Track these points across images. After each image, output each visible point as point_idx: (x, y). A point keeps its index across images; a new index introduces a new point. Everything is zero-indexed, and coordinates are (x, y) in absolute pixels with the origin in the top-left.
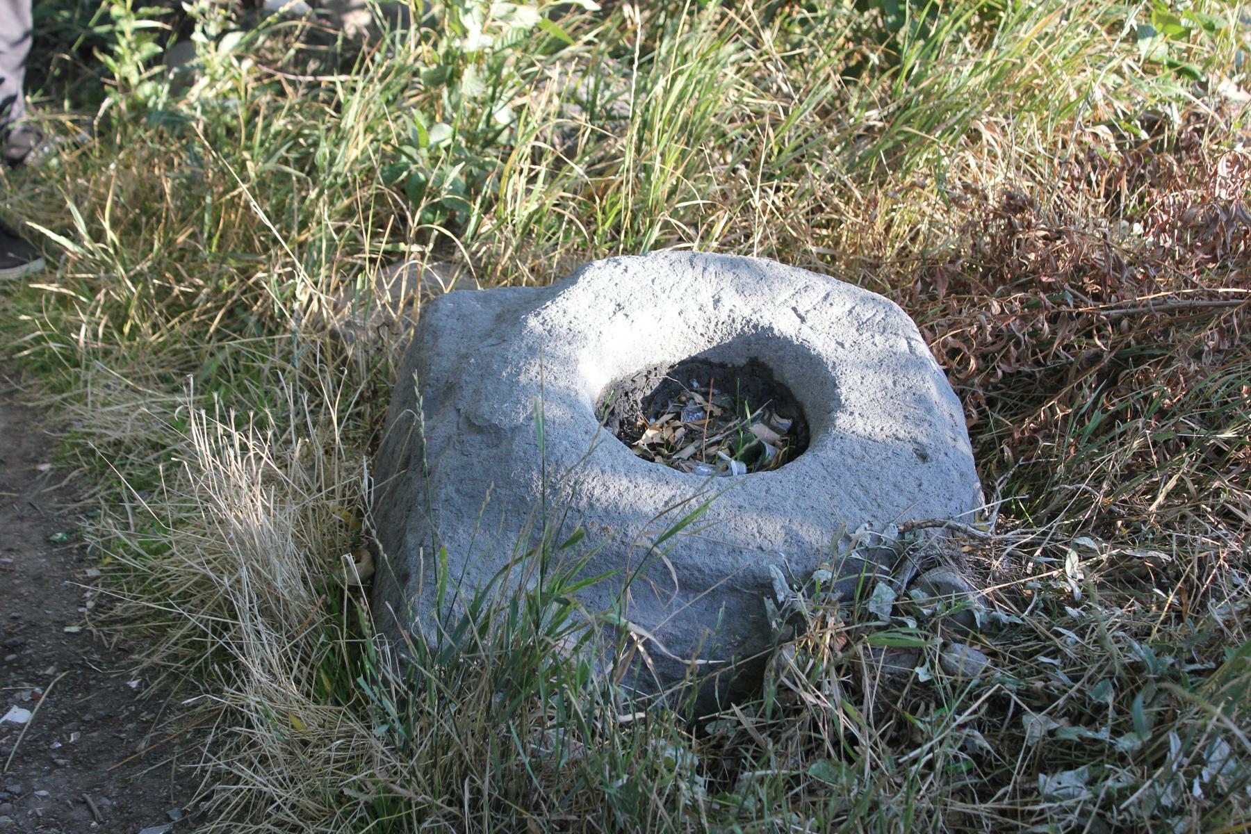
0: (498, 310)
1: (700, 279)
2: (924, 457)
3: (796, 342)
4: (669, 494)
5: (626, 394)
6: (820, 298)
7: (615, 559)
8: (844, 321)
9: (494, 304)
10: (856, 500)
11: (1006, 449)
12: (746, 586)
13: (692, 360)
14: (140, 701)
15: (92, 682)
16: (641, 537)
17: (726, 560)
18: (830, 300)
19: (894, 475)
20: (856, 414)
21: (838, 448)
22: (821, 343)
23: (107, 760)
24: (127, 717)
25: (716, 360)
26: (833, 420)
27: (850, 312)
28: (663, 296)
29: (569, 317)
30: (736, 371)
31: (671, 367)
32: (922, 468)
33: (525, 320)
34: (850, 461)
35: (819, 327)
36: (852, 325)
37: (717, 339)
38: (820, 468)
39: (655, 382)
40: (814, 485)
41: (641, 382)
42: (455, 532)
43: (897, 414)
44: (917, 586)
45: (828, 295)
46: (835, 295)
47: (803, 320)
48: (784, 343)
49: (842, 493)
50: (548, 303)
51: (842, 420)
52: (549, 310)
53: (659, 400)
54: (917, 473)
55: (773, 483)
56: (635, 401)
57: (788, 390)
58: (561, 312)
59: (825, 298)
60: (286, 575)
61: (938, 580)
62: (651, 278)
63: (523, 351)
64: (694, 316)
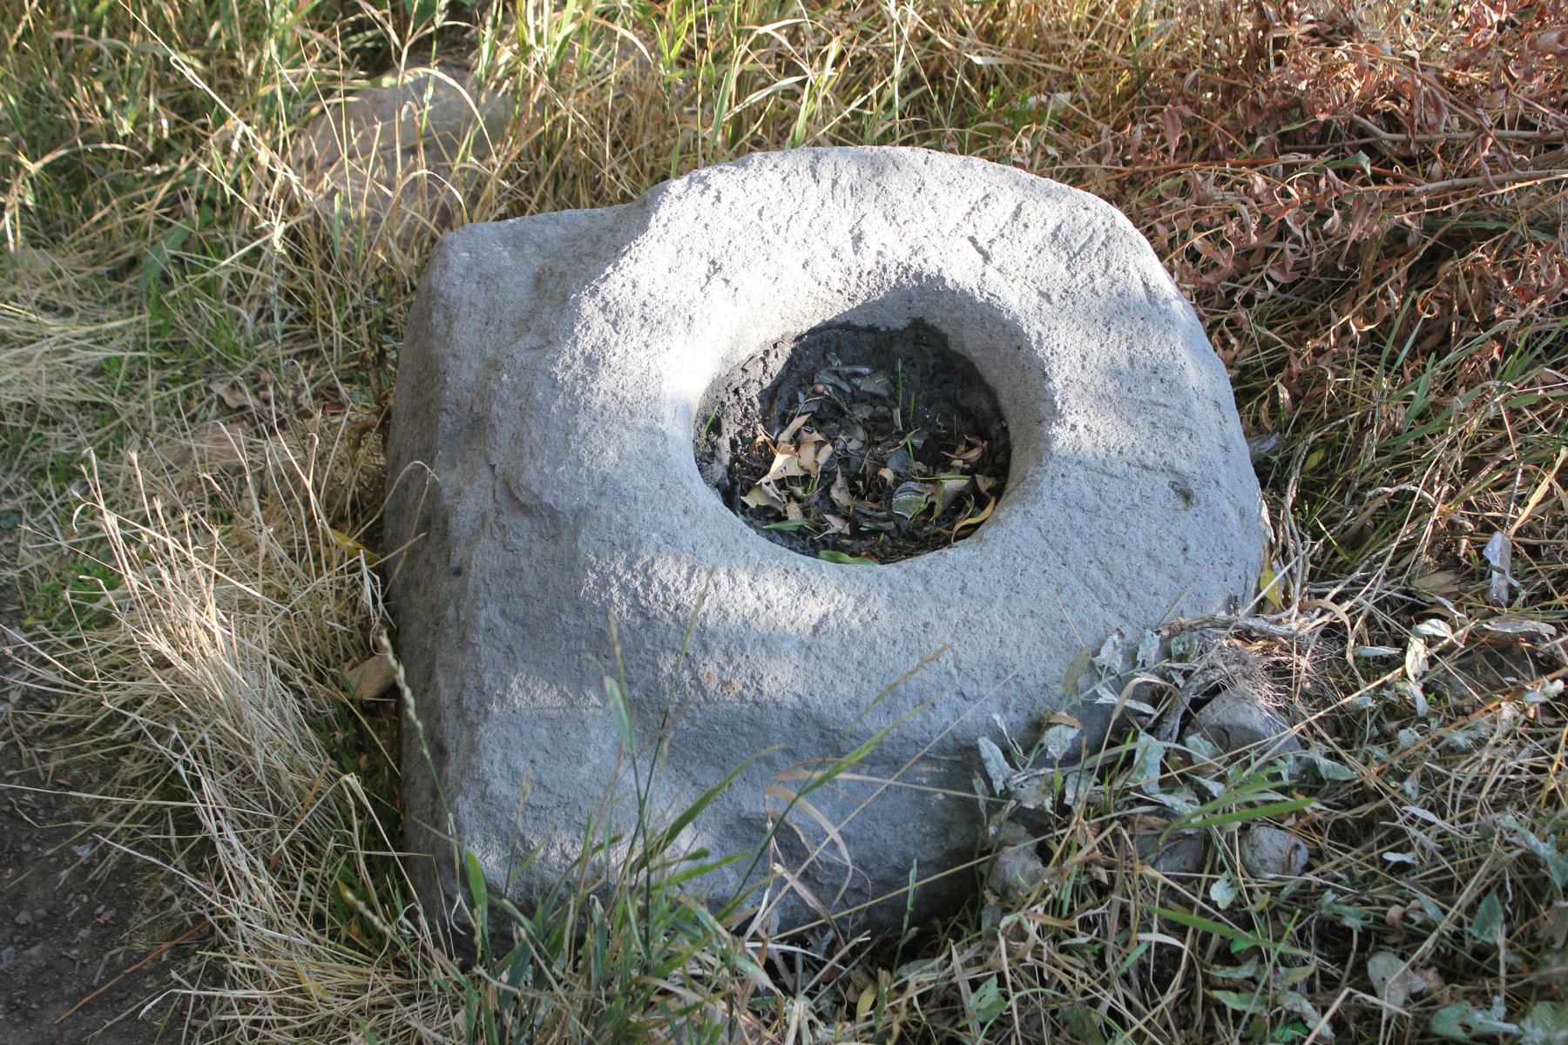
0: (537, 262)
1: (829, 202)
2: (1187, 496)
3: (980, 300)
4: (818, 612)
5: (736, 392)
6: (1007, 217)
7: (746, 729)
8: (1047, 254)
9: (529, 250)
10: (1095, 589)
11: (1281, 388)
12: (944, 751)
13: (828, 326)
14: (93, 883)
15: (26, 848)
16: (782, 680)
17: (911, 717)
18: (1023, 218)
19: (1147, 538)
20: (1081, 429)
21: (1059, 495)
22: (1015, 298)
23: (55, 1001)
24: (77, 915)
25: (862, 322)
26: (1048, 441)
27: (1055, 236)
28: (778, 240)
29: (642, 293)
30: (892, 336)
31: (799, 338)
32: (1188, 523)
33: (578, 301)
34: (1079, 519)
35: (1011, 268)
36: (1060, 259)
37: (862, 296)
38: (1037, 537)
39: (777, 365)
40: (1031, 570)
41: (756, 371)
42: (506, 687)
43: (1139, 421)
44: (1196, 729)
45: (1019, 207)
46: (1028, 207)
47: (987, 258)
48: (960, 300)
49: (1073, 580)
50: (609, 270)
51: (1061, 437)
52: (609, 285)
53: (784, 392)
54: (1177, 531)
55: (970, 574)
56: (750, 400)
57: (971, 365)
58: (629, 286)
59: (1016, 215)
60: (273, 730)
61: (1227, 721)
62: (758, 207)
63: (578, 367)
64: (827, 268)
